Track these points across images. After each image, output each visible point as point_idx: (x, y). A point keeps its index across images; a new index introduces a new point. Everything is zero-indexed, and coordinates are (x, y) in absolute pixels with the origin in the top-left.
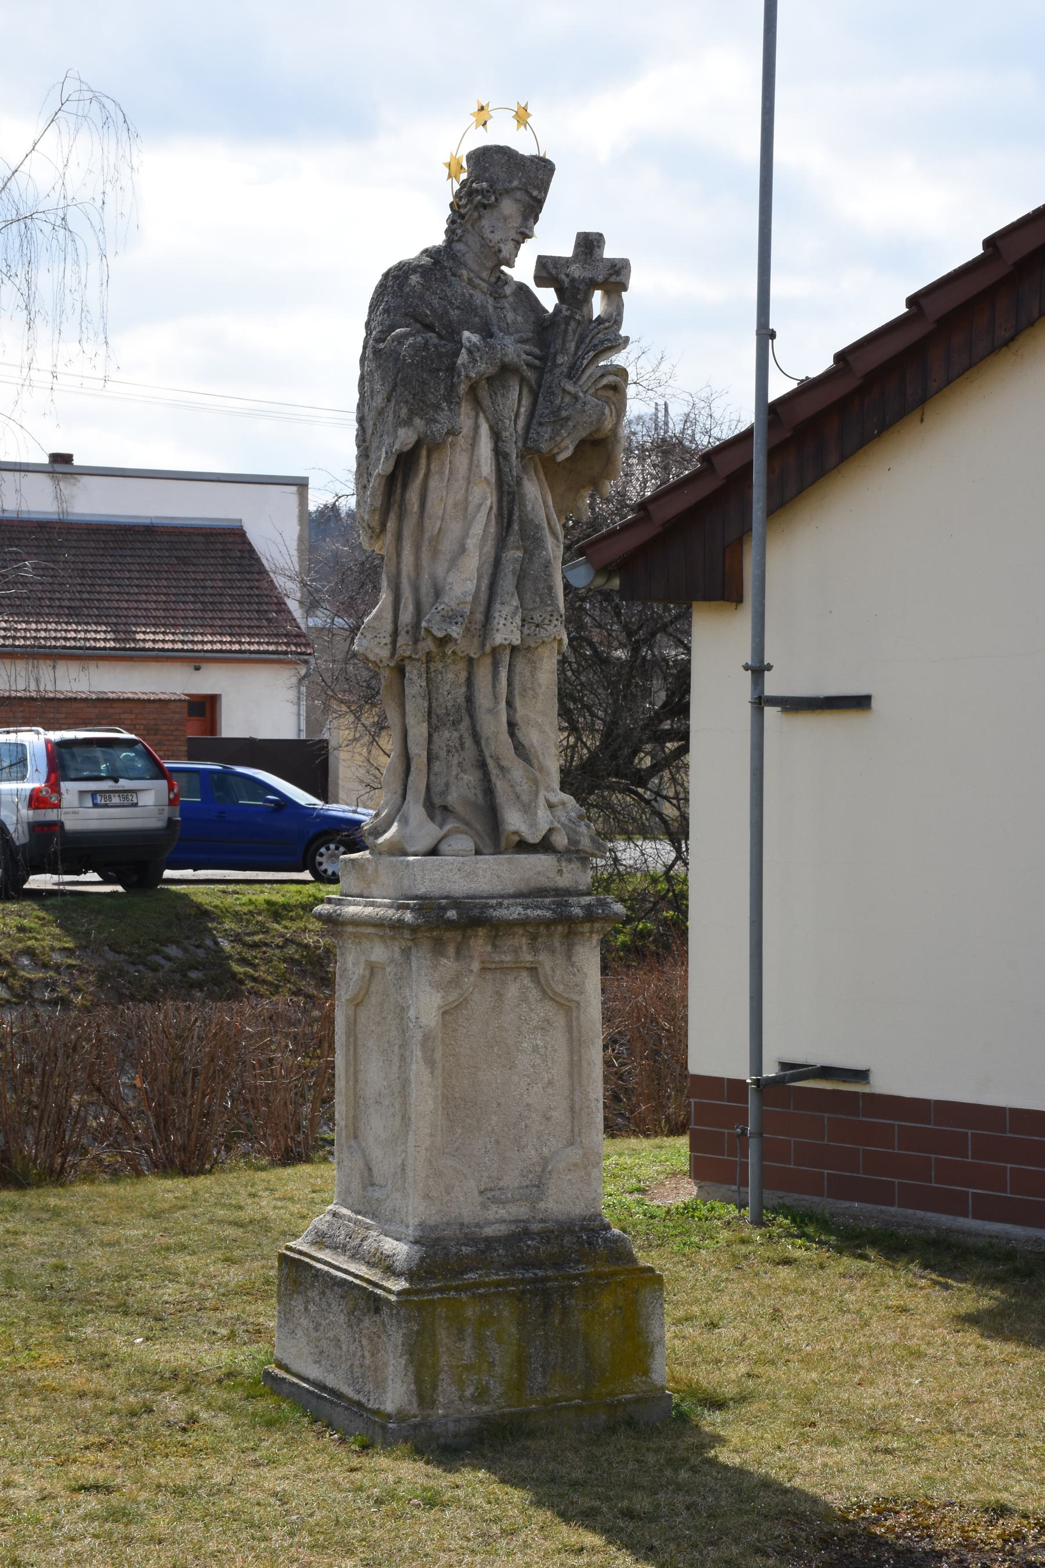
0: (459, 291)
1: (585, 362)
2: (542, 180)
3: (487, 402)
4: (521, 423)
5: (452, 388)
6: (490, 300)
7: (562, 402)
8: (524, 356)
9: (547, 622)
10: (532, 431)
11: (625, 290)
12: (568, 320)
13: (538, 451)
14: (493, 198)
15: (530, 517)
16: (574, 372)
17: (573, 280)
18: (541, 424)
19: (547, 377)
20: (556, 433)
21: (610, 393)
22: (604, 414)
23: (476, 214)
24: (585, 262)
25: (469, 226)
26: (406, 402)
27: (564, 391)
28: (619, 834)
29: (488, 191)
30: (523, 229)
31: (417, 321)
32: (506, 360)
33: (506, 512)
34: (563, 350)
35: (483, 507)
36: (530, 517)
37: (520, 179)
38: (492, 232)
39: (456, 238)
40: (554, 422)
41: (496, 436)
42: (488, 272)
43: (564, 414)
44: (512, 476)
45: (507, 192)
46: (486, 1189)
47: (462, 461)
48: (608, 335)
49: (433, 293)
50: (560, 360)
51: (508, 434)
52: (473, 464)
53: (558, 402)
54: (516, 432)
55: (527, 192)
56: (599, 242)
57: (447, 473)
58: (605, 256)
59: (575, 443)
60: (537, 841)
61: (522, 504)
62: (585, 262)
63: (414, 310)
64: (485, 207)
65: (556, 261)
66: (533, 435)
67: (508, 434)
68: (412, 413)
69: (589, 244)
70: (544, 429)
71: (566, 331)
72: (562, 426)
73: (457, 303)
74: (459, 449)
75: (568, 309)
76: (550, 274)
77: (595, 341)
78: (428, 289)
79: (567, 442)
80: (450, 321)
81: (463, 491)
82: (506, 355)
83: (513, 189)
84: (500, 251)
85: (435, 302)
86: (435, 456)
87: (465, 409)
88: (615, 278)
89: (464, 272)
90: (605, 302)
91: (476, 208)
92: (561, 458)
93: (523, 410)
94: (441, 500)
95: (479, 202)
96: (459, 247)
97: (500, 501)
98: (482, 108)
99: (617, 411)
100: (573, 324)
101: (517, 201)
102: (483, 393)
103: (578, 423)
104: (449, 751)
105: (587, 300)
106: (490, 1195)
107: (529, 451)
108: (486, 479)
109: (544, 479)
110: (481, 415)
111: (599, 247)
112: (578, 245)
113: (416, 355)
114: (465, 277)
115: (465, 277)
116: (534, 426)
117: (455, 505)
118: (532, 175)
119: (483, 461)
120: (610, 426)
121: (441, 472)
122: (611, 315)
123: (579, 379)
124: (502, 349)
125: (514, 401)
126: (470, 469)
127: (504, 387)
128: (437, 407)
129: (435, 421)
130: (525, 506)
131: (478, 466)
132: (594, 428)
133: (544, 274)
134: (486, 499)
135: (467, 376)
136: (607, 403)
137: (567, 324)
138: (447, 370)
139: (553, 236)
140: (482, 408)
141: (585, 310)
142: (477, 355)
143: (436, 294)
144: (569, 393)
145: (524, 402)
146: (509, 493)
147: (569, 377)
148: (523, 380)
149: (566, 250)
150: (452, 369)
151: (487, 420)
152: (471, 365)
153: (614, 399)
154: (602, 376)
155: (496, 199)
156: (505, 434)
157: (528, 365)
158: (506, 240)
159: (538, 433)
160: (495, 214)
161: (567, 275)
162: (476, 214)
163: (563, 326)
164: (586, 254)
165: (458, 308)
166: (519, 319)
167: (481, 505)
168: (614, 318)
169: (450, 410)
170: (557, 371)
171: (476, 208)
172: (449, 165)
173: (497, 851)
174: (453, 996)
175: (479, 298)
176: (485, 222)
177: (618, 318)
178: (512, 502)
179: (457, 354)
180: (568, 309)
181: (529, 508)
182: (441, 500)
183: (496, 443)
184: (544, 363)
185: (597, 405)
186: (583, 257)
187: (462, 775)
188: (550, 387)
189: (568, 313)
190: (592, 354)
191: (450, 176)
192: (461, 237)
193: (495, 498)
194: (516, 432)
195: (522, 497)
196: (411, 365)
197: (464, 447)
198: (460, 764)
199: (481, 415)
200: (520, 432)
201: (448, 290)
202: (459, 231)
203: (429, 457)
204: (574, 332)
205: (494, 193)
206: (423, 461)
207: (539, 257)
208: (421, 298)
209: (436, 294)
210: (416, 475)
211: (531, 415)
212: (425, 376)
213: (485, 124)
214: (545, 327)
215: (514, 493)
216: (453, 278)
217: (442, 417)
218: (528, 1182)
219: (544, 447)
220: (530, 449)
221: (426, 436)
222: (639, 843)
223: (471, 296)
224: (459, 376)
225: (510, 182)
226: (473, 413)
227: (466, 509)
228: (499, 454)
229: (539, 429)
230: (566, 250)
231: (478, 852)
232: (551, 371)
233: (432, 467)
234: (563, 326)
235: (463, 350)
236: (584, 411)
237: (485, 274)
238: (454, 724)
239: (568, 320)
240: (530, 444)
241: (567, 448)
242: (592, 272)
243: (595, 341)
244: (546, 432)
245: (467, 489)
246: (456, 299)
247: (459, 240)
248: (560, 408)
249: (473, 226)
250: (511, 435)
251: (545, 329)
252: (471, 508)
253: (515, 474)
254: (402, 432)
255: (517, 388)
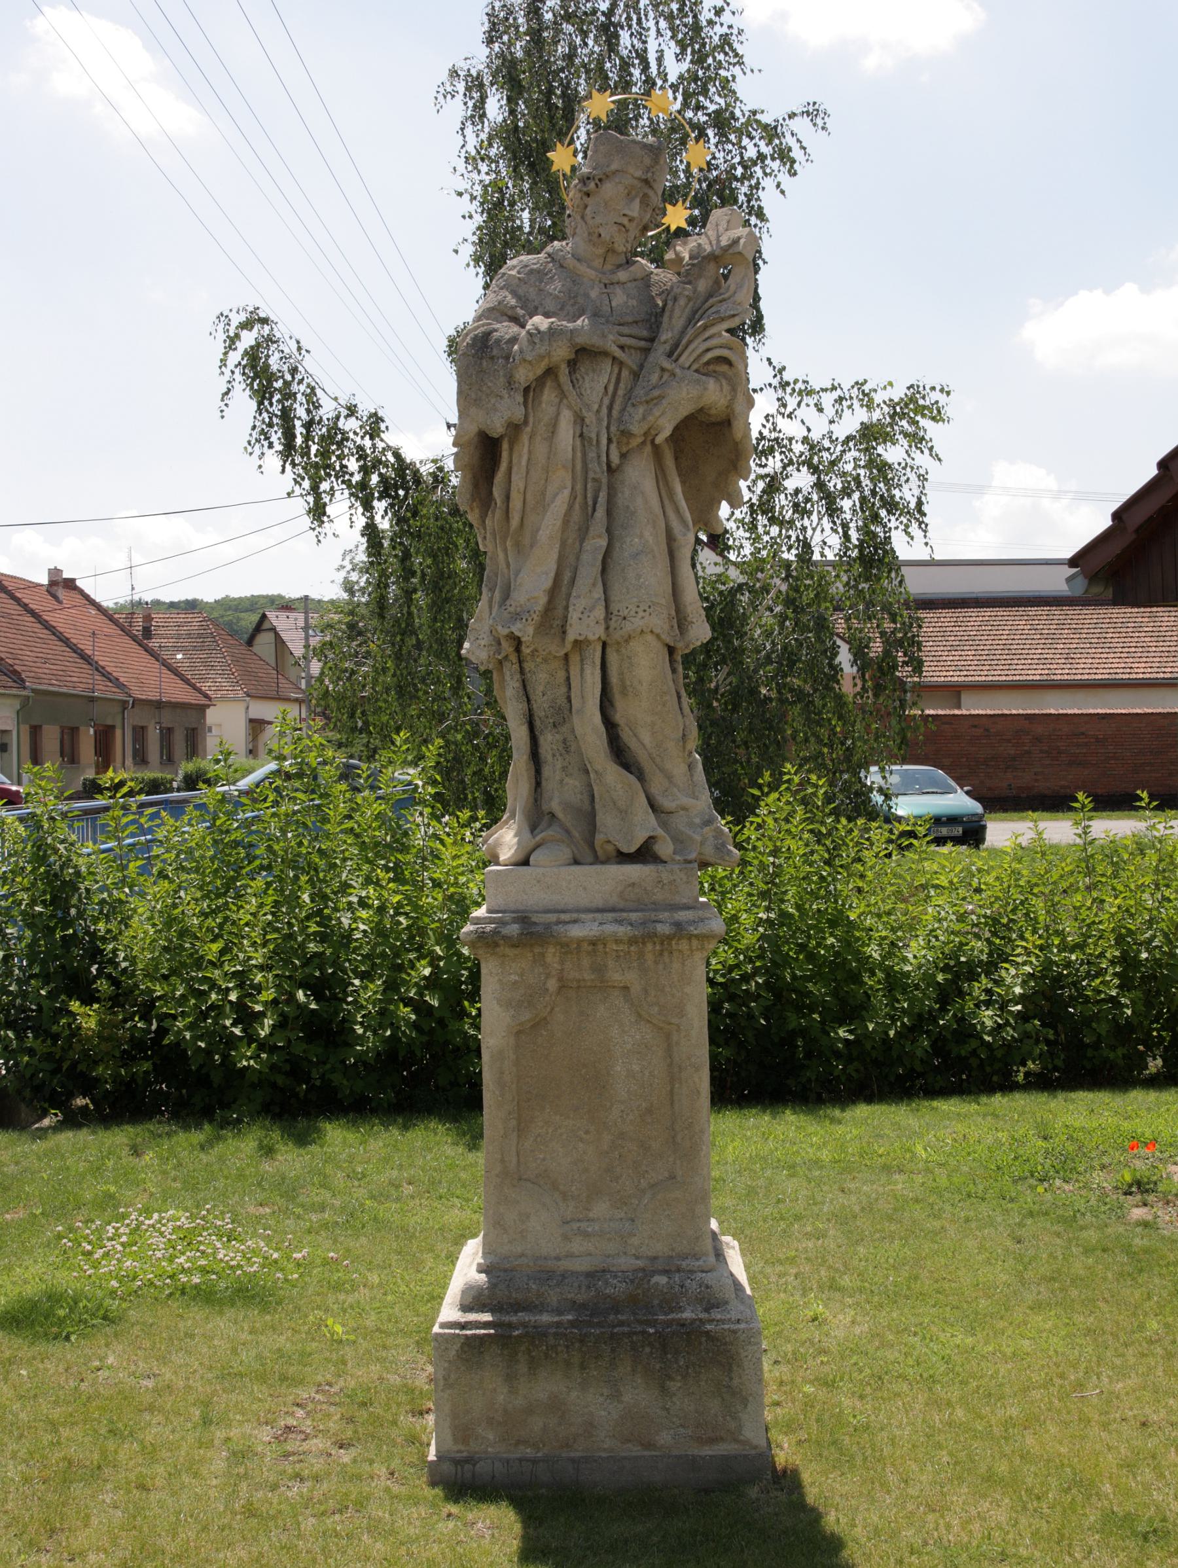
9: (633, 613)
33: (590, 503)
41: (580, 420)
46: (573, 1220)
60: (633, 850)
104: (554, 755)
106: (575, 1225)
127: (594, 371)
173: (597, 860)
174: (526, 1016)
187: (567, 780)
198: (564, 768)
203: (511, 449)
218: (623, 1215)
222: (885, 808)
231: (576, 862)
238: (555, 726)
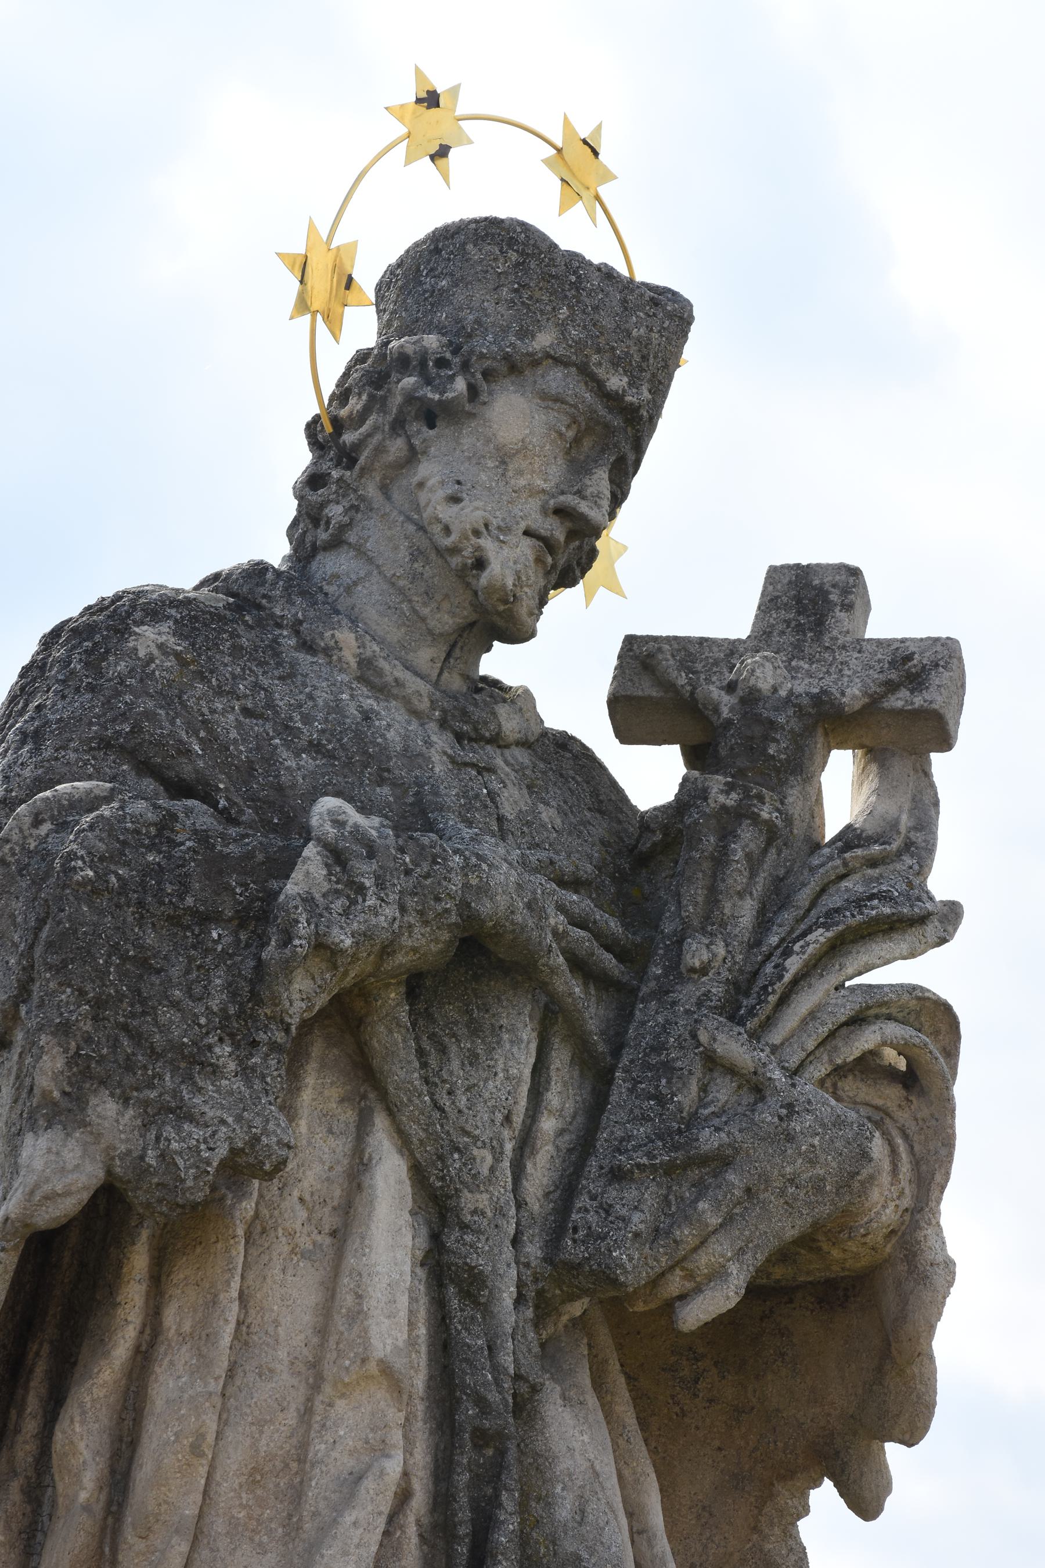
0: (323, 697)
1: (793, 965)
2: (643, 344)
3: (402, 1071)
4: (540, 1172)
5: (255, 990)
6: (442, 741)
7: (702, 1103)
8: (557, 920)
10: (583, 1201)
11: (945, 743)
12: (729, 821)
13: (607, 1278)
14: (460, 385)
15: (569, 1546)
16: (747, 1000)
17: (751, 699)
18: (617, 1175)
19: (649, 1014)
20: (673, 1214)
21: (891, 1095)
22: (865, 1156)
23: (397, 447)
24: (797, 651)
25: (371, 490)
26: (64, 1029)
27: (712, 1061)
28: (342, 951)
29: (442, 363)
30: (569, 500)
31: (145, 768)
32: (484, 907)
33: (464, 1515)
34: (712, 921)
35: (369, 1484)
36: (569, 1546)
37: (562, 327)
38: (455, 499)
39: (323, 536)
40: (669, 1169)
41: (437, 1204)
42: (438, 652)
43: (709, 1140)
44: (497, 1369)
45: (515, 367)
47: (290, 1296)
48: (888, 891)
49: (219, 692)
50: (697, 952)
51: (483, 1200)
52: (336, 1309)
53: (687, 1097)
54: (520, 1204)
55: (585, 371)
56: (846, 591)
57: (226, 1338)
58: (868, 635)
59: (755, 1259)
61: (535, 1497)
62: (797, 651)
63: (136, 730)
64: (430, 417)
65: (690, 651)
66: (585, 1213)
67: (483, 1200)
68: (86, 1074)
69: (810, 601)
70: (631, 1194)
71: (720, 860)
72: (701, 1189)
73: (309, 733)
74: (283, 1247)
75: (730, 788)
76: (669, 686)
77: (833, 900)
78: (201, 676)
79: (721, 1248)
80: (280, 788)
81: (291, 1418)
82: (483, 890)
83: (535, 362)
84: (480, 564)
85: (228, 724)
86: (182, 1272)
87: (319, 1092)
88: (908, 706)
89: (346, 637)
90: (871, 783)
91: (398, 426)
92: (695, 1314)
93: (548, 1125)
94: (196, 1450)
95: (410, 398)
96: (334, 564)
97: (443, 1470)
98: (431, 100)
99: (916, 1163)
100: (748, 838)
101: (551, 399)
102: (392, 1037)
103: (765, 1178)
105: (803, 768)
107: (569, 1278)
108: (386, 1370)
109: (630, 1419)
110: (380, 1122)
111: (848, 607)
112: (769, 604)
113: (115, 857)
114: (349, 656)
115: (349, 656)
116: (592, 1182)
117: (255, 1476)
118: (607, 322)
119: (377, 1294)
120: (889, 1216)
121: (203, 1337)
122: (894, 825)
123: (768, 1023)
124: (466, 868)
125: (509, 1080)
126: (323, 1331)
127: (475, 1029)
128: (195, 1062)
129: (184, 1114)
130: (548, 1502)
131: (357, 1315)
132: (825, 1210)
133: (647, 689)
134: (382, 1450)
135: (321, 946)
136: (878, 1124)
137: (726, 835)
138: (242, 919)
139: (683, 556)
140: (383, 1096)
141: (793, 795)
142: (365, 871)
143: (233, 694)
144: (732, 1070)
145: (553, 1097)
146: (482, 1438)
147: (733, 1013)
148: (552, 1016)
149: (729, 613)
150: (260, 916)
151: (404, 1142)
152: (338, 905)
153: (903, 1116)
154: (858, 1021)
155: (473, 391)
156: (469, 1201)
157: (578, 964)
158: (504, 529)
159: (608, 1210)
160: (467, 441)
161: (731, 688)
162: (397, 447)
163: (710, 841)
164: (800, 629)
165: (315, 747)
166: (547, 814)
167: (357, 1478)
168: (904, 838)
169: (245, 1072)
170: (687, 994)
171: (398, 426)
172: (302, 268)
175: (394, 726)
176: (428, 470)
177: (918, 837)
178: (492, 1475)
179: (284, 865)
180: (730, 788)
181: (564, 1512)
182: (196, 1450)
183: (436, 1239)
184: (633, 964)
185: (839, 1122)
186: (790, 638)
188: (658, 1048)
189: (731, 800)
190: (820, 937)
191: (302, 305)
192: (343, 528)
193: (421, 1457)
194: (520, 1204)
195: (538, 1467)
196: (94, 890)
197: (304, 1242)
199: (380, 1122)
200: (535, 1205)
201: (279, 689)
202: (335, 512)
204: (754, 864)
205: (465, 366)
206: (133, 1294)
207: (630, 641)
208: (172, 698)
209: (233, 694)
210: (102, 1345)
211: (582, 1147)
212: (150, 938)
213: (441, 153)
214: (643, 853)
215: (500, 1436)
216: (304, 658)
217: (211, 1100)
219: (631, 1262)
220: (574, 1267)
221: (142, 1171)
223: (367, 716)
224: (287, 940)
225: (524, 334)
226: (348, 1116)
227: (297, 1495)
228: (447, 1276)
229: (612, 1193)
230: (729, 613)
232: (662, 993)
233: (170, 1317)
234: (710, 841)
235: (311, 850)
236: (790, 1138)
237: (426, 656)
239: (729, 821)
240: (572, 1250)
241: (719, 1274)
242: (822, 685)
243: (833, 900)
244: (639, 1206)
245: (307, 1412)
246: (307, 719)
247: (336, 543)
248: (693, 1121)
249: (385, 489)
250: (500, 1212)
251: (643, 860)
252: (320, 1487)
253: (507, 1360)
254: (37, 1150)
255: (528, 1035)
